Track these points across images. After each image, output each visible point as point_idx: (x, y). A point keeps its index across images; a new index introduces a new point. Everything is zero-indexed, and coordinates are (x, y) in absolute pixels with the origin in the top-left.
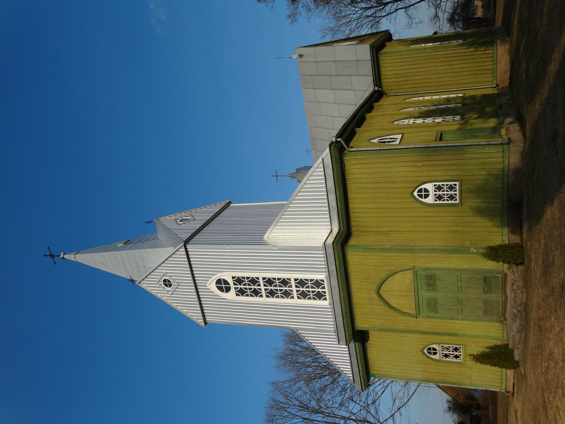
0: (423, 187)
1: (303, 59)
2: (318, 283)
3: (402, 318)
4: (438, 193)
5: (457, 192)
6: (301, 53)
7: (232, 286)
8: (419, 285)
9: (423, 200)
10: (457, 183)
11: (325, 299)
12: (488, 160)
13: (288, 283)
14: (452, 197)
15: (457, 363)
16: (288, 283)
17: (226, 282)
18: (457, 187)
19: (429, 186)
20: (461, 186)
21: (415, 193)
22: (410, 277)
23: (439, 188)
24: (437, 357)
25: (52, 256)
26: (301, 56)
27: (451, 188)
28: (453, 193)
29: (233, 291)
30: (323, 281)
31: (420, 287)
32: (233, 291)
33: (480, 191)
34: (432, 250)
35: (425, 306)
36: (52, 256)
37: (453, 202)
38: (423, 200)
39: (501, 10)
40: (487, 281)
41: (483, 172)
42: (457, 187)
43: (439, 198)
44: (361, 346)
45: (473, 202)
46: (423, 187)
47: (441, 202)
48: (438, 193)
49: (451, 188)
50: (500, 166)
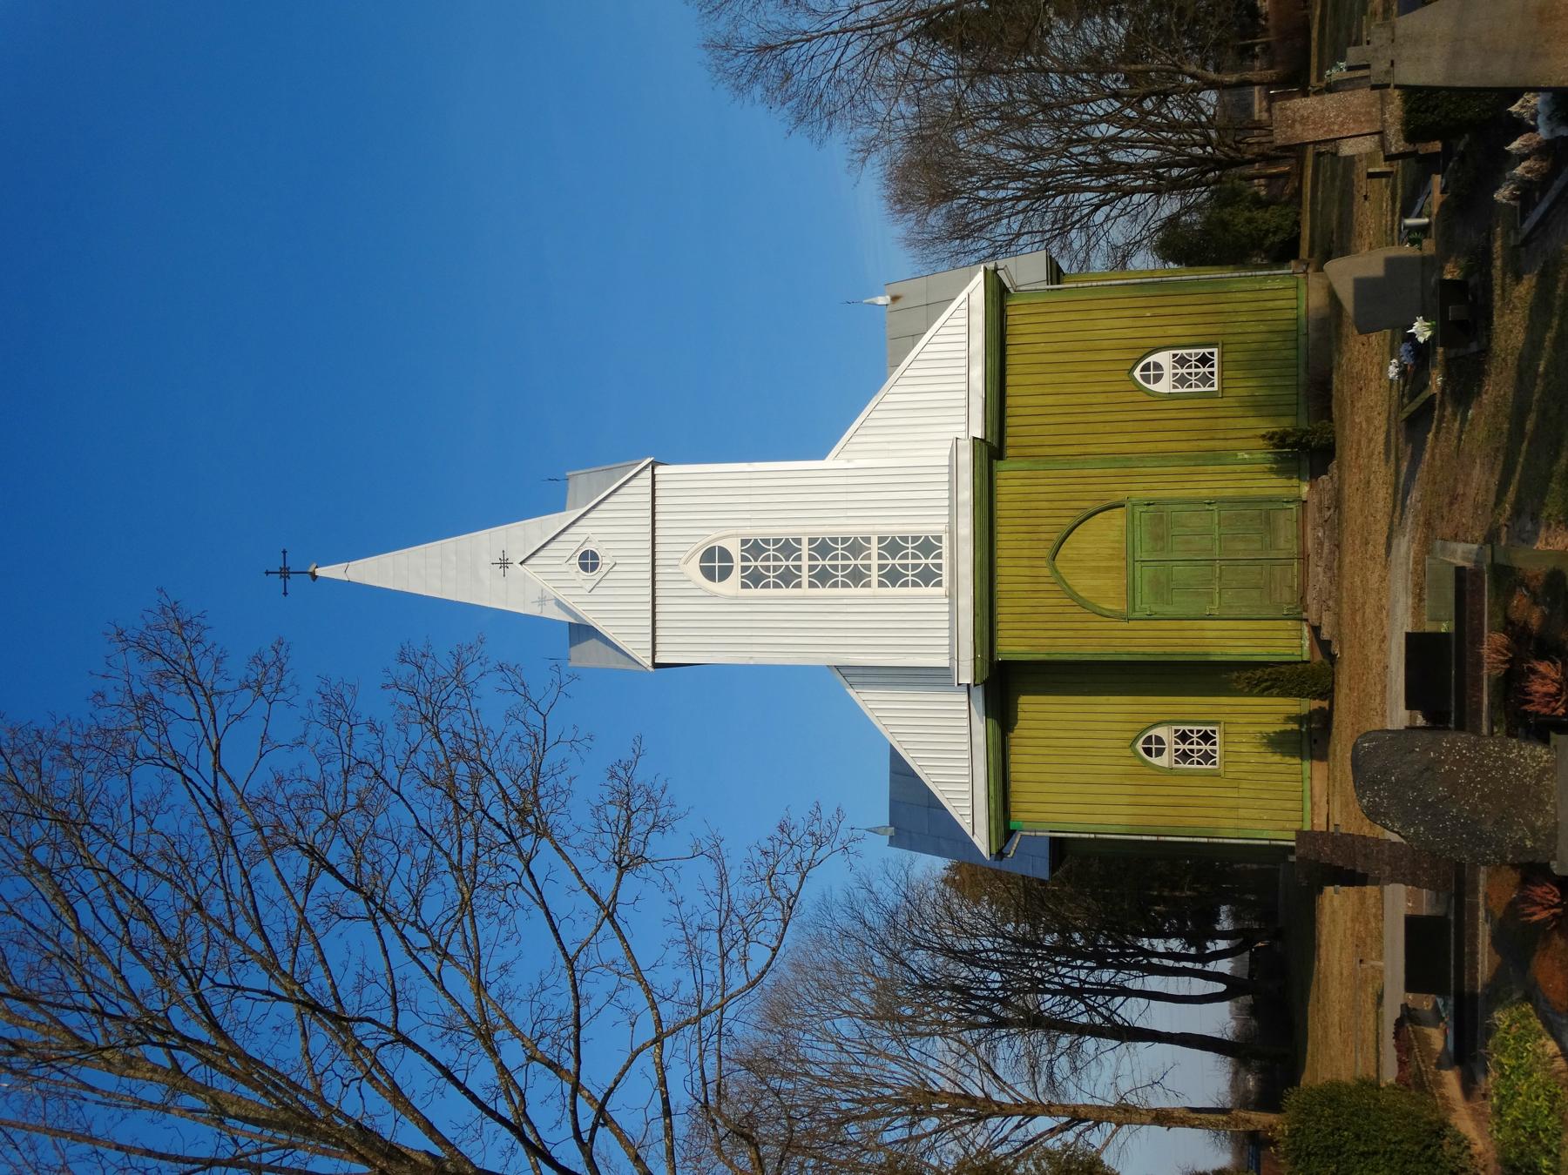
0: (1154, 732)
1: (899, 305)
2: (928, 546)
3: (1098, 624)
4: (1180, 371)
5: (1215, 369)
6: (896, 292)
7: (737, 564)
8: (1137, 538)
9: (1152, 387)
10: (1215, 350)
11: (939, 584)
12: (1270, 305)
13: (862, 549)
14: (1205, 379)
15: (1208, 774)
16: (862, 549)
17: (725, 555)
18: (1216, 357)
19: (1164, 358)
20: (1222, 354)
21: (1137, 373)
22: (1119, 523)
23: (1182, 361)
24: (1163, 761)
25: (285, 573)
26: (895, 299)
27: (1204, 360)
28: (1207, 370)
29: (736, 576)
30: (939, 539)
31: (1137, 543)
32: (736, 576)
33: (1254, 361)
34: (1164, 457)
35: (1146, 589)
36: (285, 573)
37: (1207, 389)
38: (1154, 760)
39: (1487, 940)
40: (1263, 510)
41: (1262, 328)
42: (1216, 357)
43: (1182, 380)
44: (998, 731)
45: (1244, 387)
46: (1154, 732)
47: (1204, 728)
48: (1180, 371)
49: (1204, 360)
50: (1291, 315)
